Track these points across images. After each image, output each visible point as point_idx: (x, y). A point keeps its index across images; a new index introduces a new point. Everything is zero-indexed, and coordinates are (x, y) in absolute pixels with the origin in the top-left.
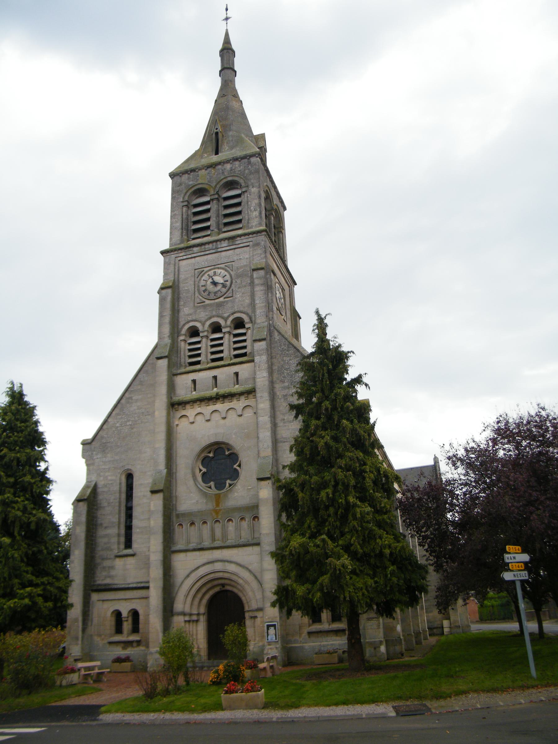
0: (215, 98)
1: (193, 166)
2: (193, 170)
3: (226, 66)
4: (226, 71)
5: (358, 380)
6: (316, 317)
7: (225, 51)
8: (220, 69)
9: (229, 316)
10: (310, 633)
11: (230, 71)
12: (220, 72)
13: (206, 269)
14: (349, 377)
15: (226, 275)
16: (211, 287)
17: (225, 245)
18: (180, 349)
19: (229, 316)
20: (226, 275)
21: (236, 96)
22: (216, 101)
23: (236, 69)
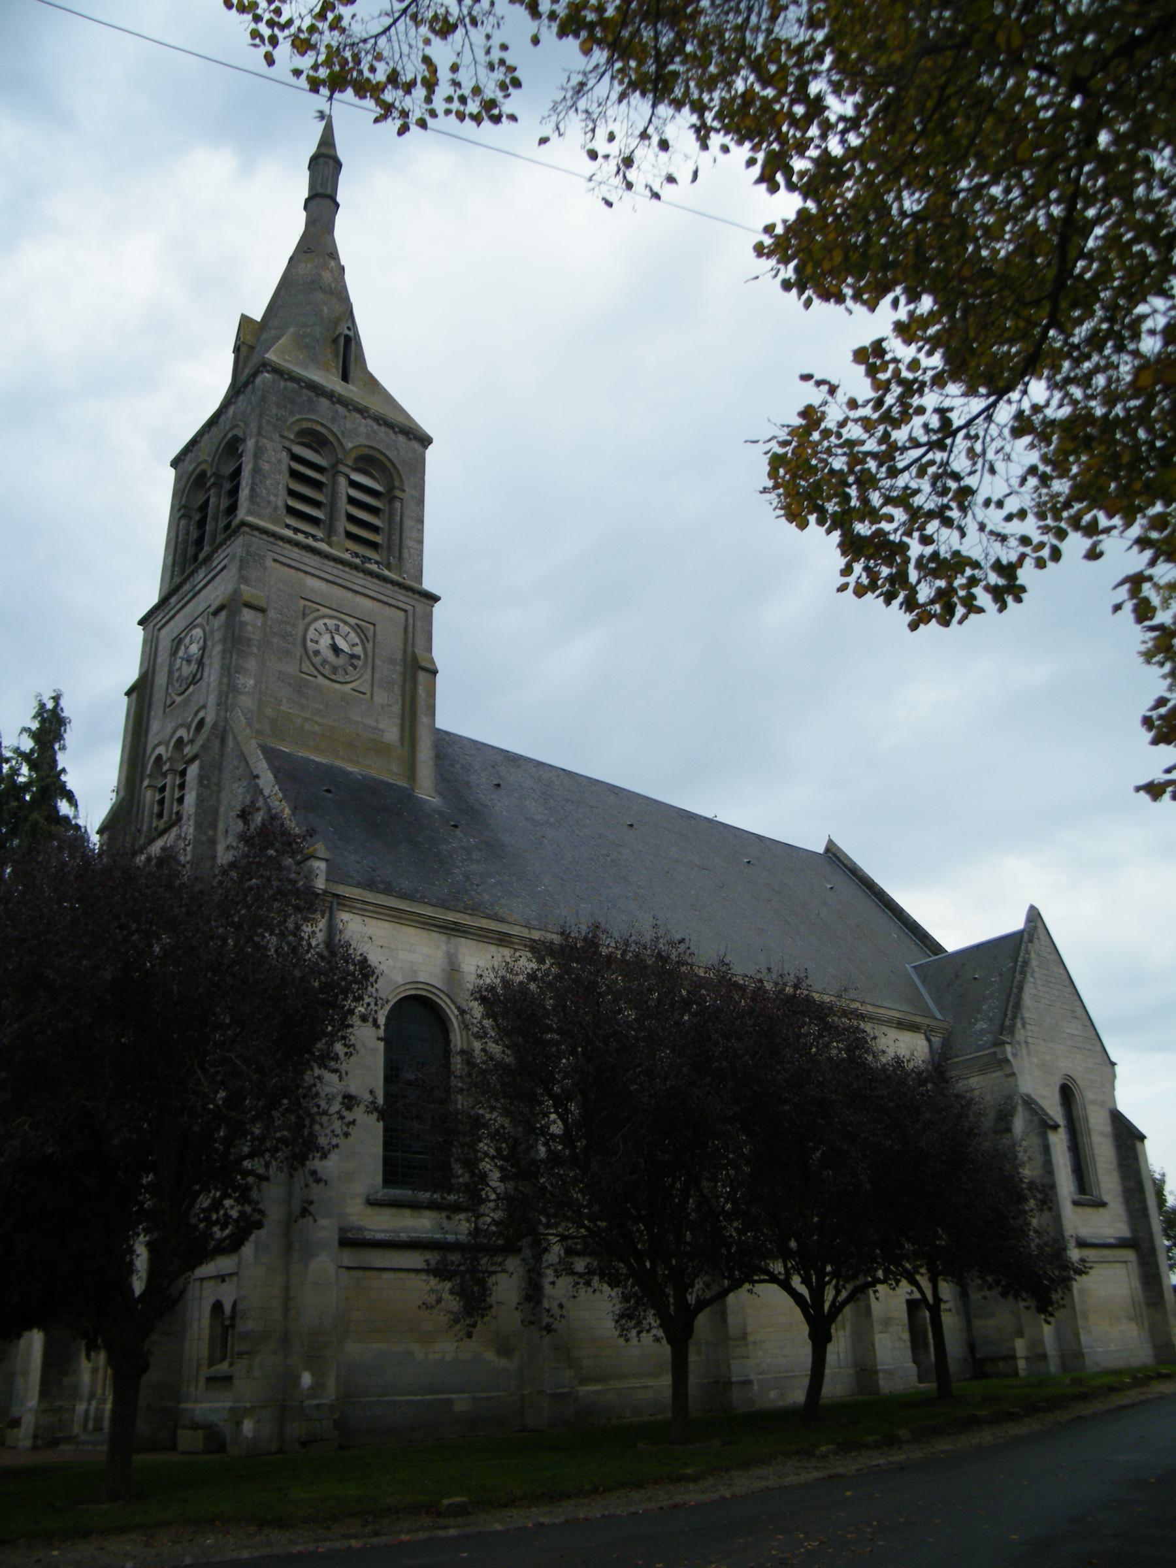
0: (290, 253)
1: (243, 379)
2: (246, 385)
3: (320, 191)
4: (318, 200)
5: (64, 770)
6: (1142, 793)
7: (321, 160)
8: (306, 195)
9: (192, 721)
10: (210, 1380)
11: (328, 202)
12: (307, 201)
13: (324, 611)
14: (60, 768)
15: (316, 630)
16: (329, 655)
17: (201, 576)
18: (144, 803)
19: (192, 721)
20: (316, 630)
21: (333, 254)
22: (291, 259)
23: (339, 199)
